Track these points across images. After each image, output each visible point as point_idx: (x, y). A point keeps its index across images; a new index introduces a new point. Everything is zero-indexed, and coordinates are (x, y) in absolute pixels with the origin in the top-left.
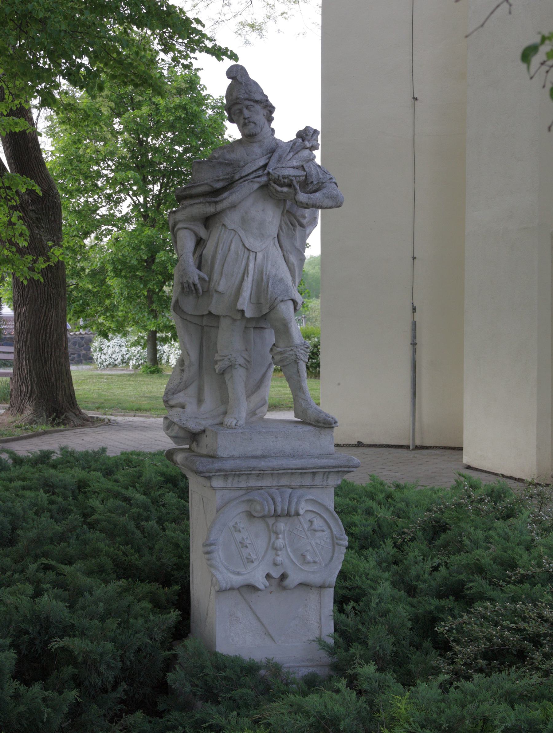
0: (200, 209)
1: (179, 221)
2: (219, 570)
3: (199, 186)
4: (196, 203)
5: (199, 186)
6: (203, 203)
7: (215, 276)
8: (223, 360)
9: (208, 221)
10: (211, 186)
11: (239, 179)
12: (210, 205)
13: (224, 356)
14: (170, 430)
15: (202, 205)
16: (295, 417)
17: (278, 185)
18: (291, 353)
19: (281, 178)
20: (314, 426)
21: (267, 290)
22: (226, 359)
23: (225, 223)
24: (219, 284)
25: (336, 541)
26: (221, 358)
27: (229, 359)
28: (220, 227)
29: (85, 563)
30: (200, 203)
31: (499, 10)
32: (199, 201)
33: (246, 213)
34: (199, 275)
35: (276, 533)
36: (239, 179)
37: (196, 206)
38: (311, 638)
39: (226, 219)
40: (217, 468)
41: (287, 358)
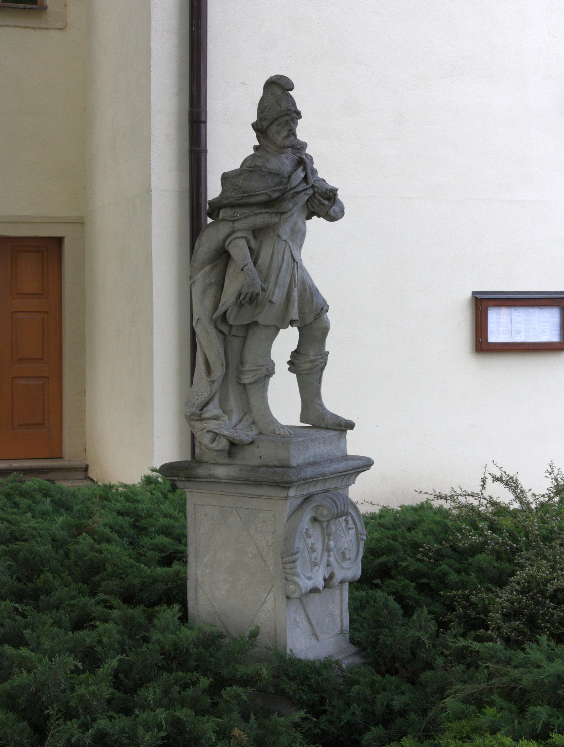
0: (261, 219)
1: (239, 230)
2: (300, 577)
3: (258, 195)
4: (261, 213)
5: (258, 195)
6: (269, 213)
7: (271, 287)
8: (260, 369)
9: (258, 232)
10: (270, 196)
11: (289, 190)
12: (276, 216)
13: (262, 366)
14: (216, 442)
15: (267, 215)
16: (302, 421)
17: (323, 198)
18: (322, 360)
19: (328, 192)
20: (336, 430)
21: (312, 301)
22: (264, 368)
23: (280, 234)
24: (273, 294)
25: (360, 536)
26: (258, 368)
27: (267, 369)
28: (275, 238)
29: (24, 587)
30: (266, 213)
31: (41, 27)
32: (265, 211)
33: (295, 224)
34: (261, 286)
35: (329, 535)
36: (289, 190)
37: (260, 216)
38: (336, 632)
39: (281, 229)
40: (303, 477)
41: (317, 365)
